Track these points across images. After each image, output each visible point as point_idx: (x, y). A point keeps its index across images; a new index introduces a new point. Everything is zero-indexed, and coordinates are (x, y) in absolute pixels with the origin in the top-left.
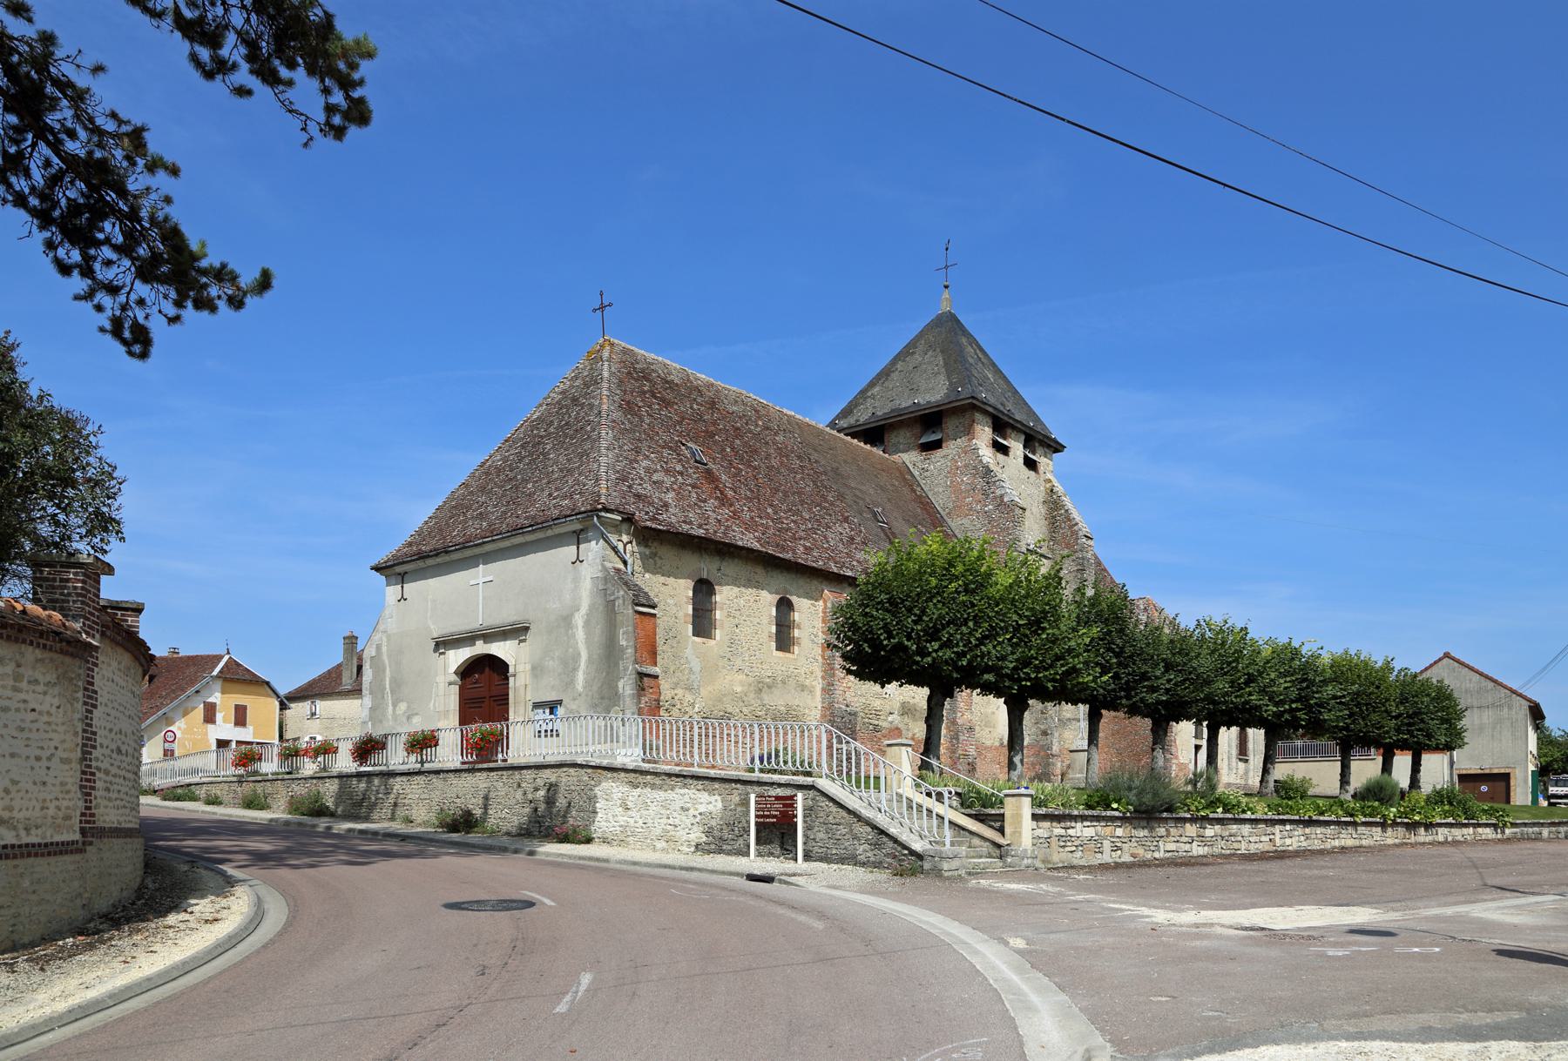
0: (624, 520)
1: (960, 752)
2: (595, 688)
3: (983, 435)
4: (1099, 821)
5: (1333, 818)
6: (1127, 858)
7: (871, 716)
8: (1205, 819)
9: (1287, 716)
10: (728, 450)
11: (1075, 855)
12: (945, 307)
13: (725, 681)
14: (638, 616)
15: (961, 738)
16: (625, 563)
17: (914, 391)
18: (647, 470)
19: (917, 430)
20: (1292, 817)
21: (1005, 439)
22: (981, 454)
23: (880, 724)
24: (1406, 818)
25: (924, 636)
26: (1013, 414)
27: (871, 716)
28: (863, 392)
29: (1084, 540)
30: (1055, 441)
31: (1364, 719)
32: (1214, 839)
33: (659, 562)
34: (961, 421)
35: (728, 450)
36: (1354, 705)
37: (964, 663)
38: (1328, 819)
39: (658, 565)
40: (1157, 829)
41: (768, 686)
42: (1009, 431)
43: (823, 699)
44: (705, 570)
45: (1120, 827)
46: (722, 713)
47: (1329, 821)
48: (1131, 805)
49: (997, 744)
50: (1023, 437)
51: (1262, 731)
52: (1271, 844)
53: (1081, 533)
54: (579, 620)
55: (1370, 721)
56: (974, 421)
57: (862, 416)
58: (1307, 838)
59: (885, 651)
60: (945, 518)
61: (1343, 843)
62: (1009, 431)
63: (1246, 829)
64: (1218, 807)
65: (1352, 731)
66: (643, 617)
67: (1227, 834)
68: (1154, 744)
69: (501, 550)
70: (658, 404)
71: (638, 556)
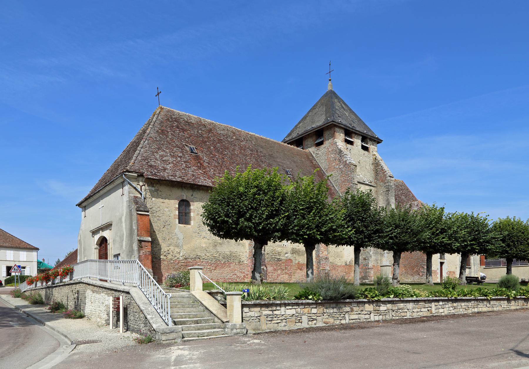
0: (138, 176)
1: (321, 268)
2: (128, 248)
3: (340, 139)
4: (299, 306)
5: (472, 297)
6: (320, 324)
7: (276, 255)
8: (379, 301)
9: (469, 248)
10: (212, 148)
11: (280, 325)
12: (329, 88)
13: (197, 242)
14: (139, 216)
15: (322, 262)
16: (141, 194)
17: (313, 122)
18: (162, 156)
19: (314, 138)
20: (443, 298)
21: (352, 138)
22: (338, 145)
23: (281, 258)
24: (524, 295)
25: (234, 215)
26: (356, 128)
27: (276, 255)
28: (296, 126)
29: (389, 178)
30: (377, 138)
31: (515, 248)
32: (387, 311)
33: (160, 193)
34: (330, 132)
35: (212, 148)
36: (511, 242)
37: (261, 228)
38: (470, 298)
39: (159, 195)
40: (344, 308)
41: (219, 244)
42: (353, 135)
43: (249, 248)
44: (185, 195)
45: (316, 308)
46: (195, 256)
47: (470, 299)
48: (321, 296)
49: (344, 264)
50: (361, 137)
51: (460, 255)
52: (429, 312)
53: (387, 175)
54: (123, 220)
55: (519, 249)
56: (335, 131)
57: (294, 135)
58: (455, 308)
59: (219, 223)
60: (325, 172)
61: (480, 310)
62: (353, 135)
63: (410, 305)
64: (392, 295)
65: (510, 253)
66: (142, 216)
67: (397, 308)
68: (394, 263)
69: (105, 193)
70: (179, 131)
71: (148, 191)
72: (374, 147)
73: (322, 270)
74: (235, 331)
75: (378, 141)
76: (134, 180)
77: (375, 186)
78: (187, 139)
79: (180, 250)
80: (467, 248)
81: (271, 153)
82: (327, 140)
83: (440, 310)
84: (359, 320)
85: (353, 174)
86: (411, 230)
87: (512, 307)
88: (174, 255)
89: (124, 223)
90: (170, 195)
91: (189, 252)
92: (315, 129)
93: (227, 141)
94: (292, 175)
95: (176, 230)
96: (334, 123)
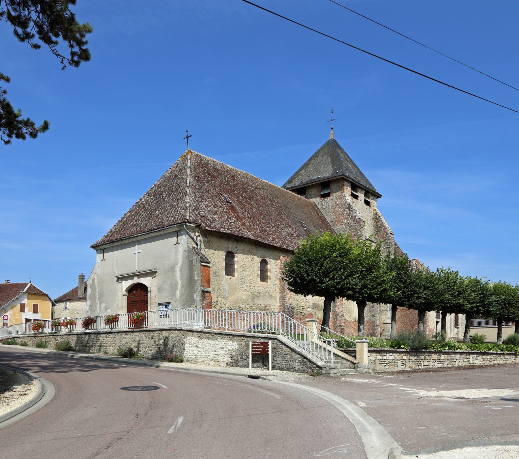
0: (196, 226)
1: (338, 324)
2: (184, 297)
4: (396, 353)
5: (494, 352)
6: (408, 369)
9: (475, 309)
10: (240, 197)
12: (331, 137)
14: (202, 267)
15: (338, 318)
16: (197, 244)
17: (318, 172)
19: (320, 189)
20: (477, 351)
21: (356, 192)
22: (346, 199)
23: (304, 312)
28: (297, 173)
30: (377, 193)
31: (507, 310)
32: (444, 360)
33: (211, 244)
34: (338, 185)
35: (240, 197)
36: (503, 304)
37: (340, 287)
39: (211, 245)
40: (421, 357)
42: (358, 189)
44: (231, 247)
45: (405, 355)
46: (238, 308)
49: (353, 321)
50: (364, 192)
51: (465, 315)
52: (469, 363)
53: (388, 232)
54: (178, 268)
56: (343, 185)
57: (297, 183)
59: (306, 281)
60: (332, 225)
61: (498, 362)
62: (358, 189)
63: (458, 356)
64: (446, 347)
70: (211, 178)
71: (202, 242)
72: (375, 202)
73: (338, 326)
74: (365, 370)
75: (378, 196)
76: (192, 230)
77: (376, 242)
78: (219, 188)
79: (226, 301)
80: (473, 309)
81: (285, 203)
82: (335, 193)
83: (475, 361)
84: (429, 367)
85: (362, 230)
86: (437, 292)
87: (517, 361)
88: (221, 306)
89: (178, 272)
90: (219, 247)
91: (233, 303)
92: (323, 180)
93: (249, 189)
94: (307, 228)
95: (223, 281)
96: (344, 177)
